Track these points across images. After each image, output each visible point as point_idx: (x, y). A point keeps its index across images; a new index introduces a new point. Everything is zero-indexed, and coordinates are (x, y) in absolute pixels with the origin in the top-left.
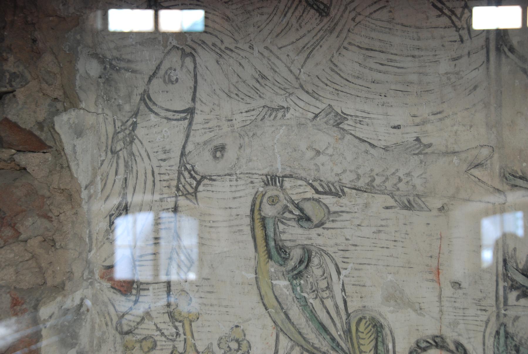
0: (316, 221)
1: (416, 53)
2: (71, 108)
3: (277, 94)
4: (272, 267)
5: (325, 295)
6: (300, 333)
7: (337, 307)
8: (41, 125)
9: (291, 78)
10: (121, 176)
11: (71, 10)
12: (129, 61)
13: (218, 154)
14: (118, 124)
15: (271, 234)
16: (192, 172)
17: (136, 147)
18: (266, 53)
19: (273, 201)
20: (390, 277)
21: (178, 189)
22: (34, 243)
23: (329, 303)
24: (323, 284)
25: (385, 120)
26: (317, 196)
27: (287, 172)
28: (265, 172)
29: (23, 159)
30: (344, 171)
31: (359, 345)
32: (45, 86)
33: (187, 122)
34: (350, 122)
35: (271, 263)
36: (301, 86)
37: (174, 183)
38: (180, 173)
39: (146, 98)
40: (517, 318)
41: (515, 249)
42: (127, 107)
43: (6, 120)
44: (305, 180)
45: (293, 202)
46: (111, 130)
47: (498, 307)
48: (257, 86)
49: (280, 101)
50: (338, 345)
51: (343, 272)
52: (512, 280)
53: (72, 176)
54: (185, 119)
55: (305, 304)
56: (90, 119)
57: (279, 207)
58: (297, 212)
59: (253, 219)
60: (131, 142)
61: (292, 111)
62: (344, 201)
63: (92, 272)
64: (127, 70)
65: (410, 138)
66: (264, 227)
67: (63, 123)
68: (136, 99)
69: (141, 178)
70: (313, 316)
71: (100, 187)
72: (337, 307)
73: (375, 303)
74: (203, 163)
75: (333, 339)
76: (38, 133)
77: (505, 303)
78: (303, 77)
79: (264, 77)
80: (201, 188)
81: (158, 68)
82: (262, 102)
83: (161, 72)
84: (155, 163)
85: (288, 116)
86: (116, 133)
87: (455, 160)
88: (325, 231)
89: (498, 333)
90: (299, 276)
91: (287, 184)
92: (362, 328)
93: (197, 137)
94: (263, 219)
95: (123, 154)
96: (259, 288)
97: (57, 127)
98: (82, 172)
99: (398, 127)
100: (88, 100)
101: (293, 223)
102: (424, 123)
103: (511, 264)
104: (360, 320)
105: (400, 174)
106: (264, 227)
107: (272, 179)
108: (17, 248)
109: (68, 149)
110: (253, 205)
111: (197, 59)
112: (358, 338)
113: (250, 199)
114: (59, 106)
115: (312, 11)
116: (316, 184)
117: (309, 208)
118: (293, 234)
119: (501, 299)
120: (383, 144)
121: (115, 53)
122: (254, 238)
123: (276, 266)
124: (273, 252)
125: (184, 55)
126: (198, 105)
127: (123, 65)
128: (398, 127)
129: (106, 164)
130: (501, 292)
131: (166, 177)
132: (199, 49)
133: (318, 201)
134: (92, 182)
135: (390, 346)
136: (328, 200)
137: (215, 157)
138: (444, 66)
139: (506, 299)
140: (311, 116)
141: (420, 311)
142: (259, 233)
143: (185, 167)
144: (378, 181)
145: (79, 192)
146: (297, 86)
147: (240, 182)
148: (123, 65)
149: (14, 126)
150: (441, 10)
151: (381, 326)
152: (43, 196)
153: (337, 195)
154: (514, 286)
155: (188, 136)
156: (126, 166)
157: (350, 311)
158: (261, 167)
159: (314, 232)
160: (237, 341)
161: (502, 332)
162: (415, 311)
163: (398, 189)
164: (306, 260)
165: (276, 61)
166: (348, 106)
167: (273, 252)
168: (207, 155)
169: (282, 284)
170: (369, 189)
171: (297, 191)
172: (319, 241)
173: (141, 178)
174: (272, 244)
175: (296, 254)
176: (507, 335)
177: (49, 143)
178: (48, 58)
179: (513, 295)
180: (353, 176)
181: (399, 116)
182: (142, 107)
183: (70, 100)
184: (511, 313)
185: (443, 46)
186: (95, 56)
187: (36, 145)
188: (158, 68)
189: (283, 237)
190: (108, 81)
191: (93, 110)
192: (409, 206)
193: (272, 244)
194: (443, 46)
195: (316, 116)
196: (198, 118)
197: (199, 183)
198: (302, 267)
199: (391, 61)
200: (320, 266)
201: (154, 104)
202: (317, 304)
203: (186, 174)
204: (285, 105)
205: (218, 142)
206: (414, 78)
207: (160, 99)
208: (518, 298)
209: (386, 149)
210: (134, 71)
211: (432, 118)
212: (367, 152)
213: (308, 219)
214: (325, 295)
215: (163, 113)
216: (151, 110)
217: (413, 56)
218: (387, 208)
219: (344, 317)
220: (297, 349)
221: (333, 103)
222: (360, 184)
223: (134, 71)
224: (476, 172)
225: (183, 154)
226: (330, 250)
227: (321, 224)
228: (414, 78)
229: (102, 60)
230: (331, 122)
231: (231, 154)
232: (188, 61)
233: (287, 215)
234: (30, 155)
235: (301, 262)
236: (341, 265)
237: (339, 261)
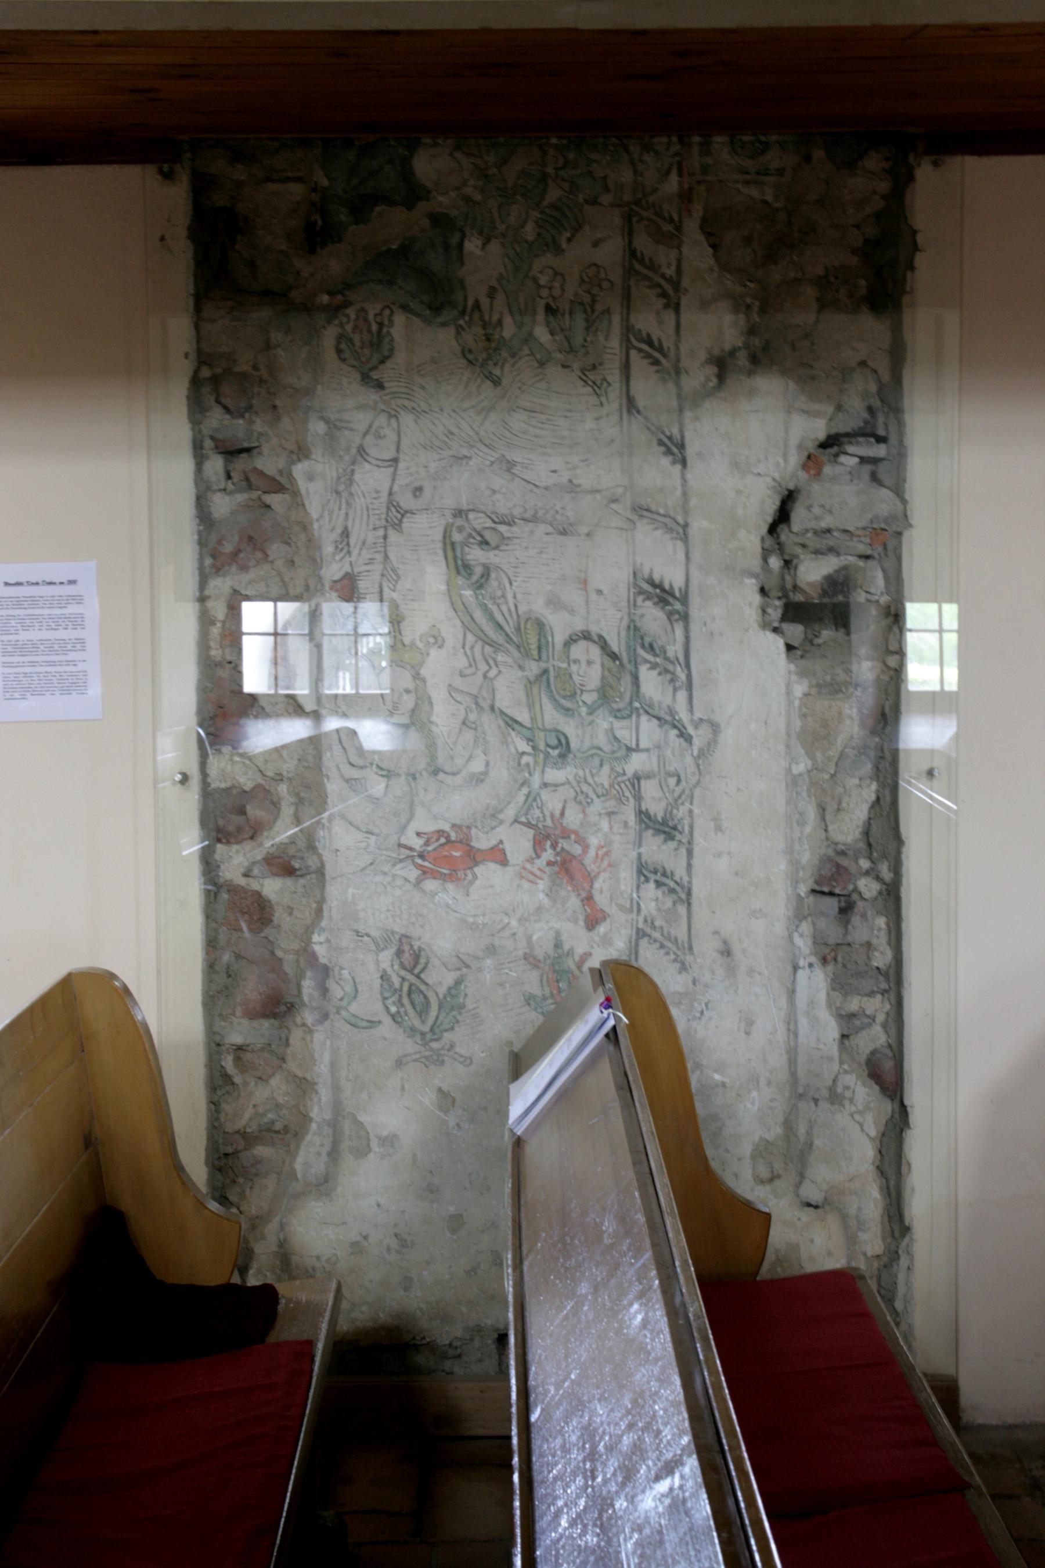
0: (493, 544)
1: (569, 414)
2: (764, 621)
3: (462, 446)
4: (460, 581)
5: (500, 601)
6: (482, 631)
7: (509, 610)
8: (281, 472)
9: (471, 433)
10: (343, 512)
11: (304, 383)
12: (348, 422)
13: (418, 494)
14: (341, 471)
15: (459, 554)
16: (397, 507)
17: (355, 488)
18: (453, 414)
19: (460, 529)
20: (550, 587)
21: (387, 521)
22: (279, 563)
23: (504, 608)
24: (499, 593)
25: (546, 468)
26: (493, 525)
27: (471, 507)
28: (453, 507)
29: (269, 499)
30: (515, 506)
31: (527, 638)
32: (283, 442)
33: (392, 469)
34: (519, 468)
35: (460, 578)
36: (481, 441)
37: (383, 516)
38: (388, 509)
39: (362, 451)
40: (642, 616)
41: (642, 564)
42: (347, 458)
43: (255, 469)
44: (485, 513)
45: (475, 530)
46: (335, 475)
47: (629, 607)
48: (447, 440)
49: (465, 452)
50: (511, 639)
51: (515, 584)
52: (640, 587)
53: (306, 511)
54: (391, 466)
55: (485, 609)
56: (319, 468)
57: (465, 534)
58: (479, 538)
59: (445, 544)
60: (351, 485)
61: (474, 460)
62: (515, 529)
63: (323, 585)
64: (346, 428)
65: (564, 480)
66: (454, 550)
67: (299, 470)
68: (354, 451)
69: (359, 512)
70: (491, 618)
71: (327, 519)
72: (509, 610)
73: (539, 607)
74: (406, 501)
75: (507, 635)
76: (278, 478)
77: (635, 605)
78: (482, 433)
79: (452, 433)
80: (405, 520)
81: (370, 426)
82: (451, 453)
83: (373, 430)
84: (369, 500)
85: (471, 463)
86: (339, 478)
87: (598, 496)
88: (501, 553)
89: (629, 627)
90: (481, 587)
91: (471, 516)
92: (529, 626)
93: (401, 481)
94: (453, 544)
95: (345, 494)
96: (450, 597)
97: (294, 474)
98: (314, 508)
99: (555, 471)
100: (317, 453)
101: (476, 547)
102: (575, 468)
103: (639, 575)
104: (527, 620)
105: (557, 508)
106: (454, 550)
107: (459, 513)
108: (266, 567)
109: (303, 491)
110: (445, 532)
111: (401, 420)
112: (526, 633)
113: (441, 529)
114: (295, 457)
115: (489, 382)
116: (494, 517)
117: (488, 535)
118: (476, 555)
119: (632, 602)
120: (543, 484)
121: (337, 416)
122: (446, 558)
123: (464, 580)
124: (461, 568)
125: (390, 416)
126: (401, 456)
127: (343, 424)
128: (555, 471)
129: (332, 502)
130: (632, 597)
131: (378, 512)
132: (402, 412)
133: (495, 529)
134: (321, 516)
135: (550, 639)
136: (502, 528)
137: (415, 496)
138: (589, 424)
139: (635, 601)
140: (488, 463)
141: (572, 612)
142: (450, 554)
143: (392, 503)
144: (541, 513)
145: (311, 524)
146: (476, 439)
147: (435, 515)
148: (343, 424)
149: (261, 473)
150: (585, 381)
151: (544, 624)
152: (284, 528)
153: (509, 524)
154: (641, 592)
155: (393, 480)
156: (347, 503)
157: (520, 613)
158: (450, 502)
159: (492, 554)
160: (434, 637)
161: (632, 627)
162: (569, 612)
163: (556, 520)
164: (486, 575)
165: (462, 422)
166: (517, 456)
167: (461, 568)
168: (409, 495)
169: (468, 593)
170: (534, 519)
171: (479, 521)
172: (496, 560)
173: (359, 512)
174: (460, 563)
175: (478, 570)
176: (636, 629)
177: (288, 486)
178: (286, 420)
179: (640, 599)
180: (521, 510)
181: (556, 463)
182: (359, 458)
183: (301, 452)
184: (639, 612)
185: (426, 467)
186: (322, 418)
187: (278, 487)
188: (370, 426)
189: (468, 557)
190: (332, 438)
191: (320, 460)
192: (564, 533)
193: (460, 563)
194: (426, 467)
195: (492, 463)
196: (402, 465)
197: (403, 516)
198: (483, 580)
199: (549, 420)
200: (497, 579)
201: (368, 455)
202: (494, 608)
203: (393, 509)
204: (468, 454)
205: (417, 484)
206: (566, 433)
207: (372, 451)
208: (644, 601)
209: (546, 488)
210: (351, 430)
211: (581, 464)
212: (531, 491)
213: (487, 543)
214: (500, 601)
215: (374, 462)
216: (365, 460)
217: (566, 417)
218: (547, 534)
219: (515, 617)
220: (480, 643)
221: (505, 453)
222: (527, 515)
223: (351, 430)
224: (614, 506)
225: (390, 494)
226: (504, 567)
227: (497, 548)
228: (566, 433)
229: (327, 421)
230: (504, 468)
231: (427, 493)
232: (393, 421)
233: (472, 540)
234: (273, 495)
235: (482, 576)
236: (513, 578)
237: (510, 575)
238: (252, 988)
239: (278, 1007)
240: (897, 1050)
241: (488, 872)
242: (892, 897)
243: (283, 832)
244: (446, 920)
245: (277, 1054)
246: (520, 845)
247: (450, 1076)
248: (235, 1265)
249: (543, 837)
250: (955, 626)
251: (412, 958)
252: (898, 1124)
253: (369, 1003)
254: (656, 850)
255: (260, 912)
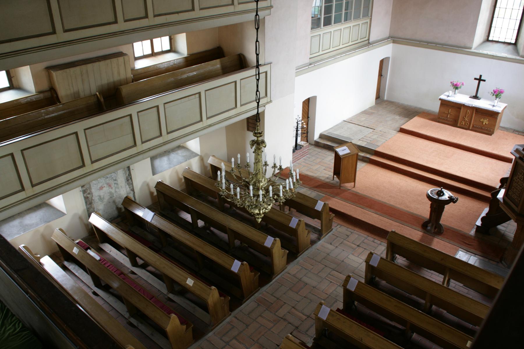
146: (67, 85)
238: (88, 203)
239: (91, 203)
240: (133, 188)
241: (104, 188)
242: (131, 178)
243: (88, 191)
244: (101, 193)
245: (91, 207)
246: (106, 185)
247: (104, 203)
248: (358, 256)
249: (107, 184)
250: (147, 43)
251: (100, 196)
252: (134, 193)
253: (98, 201)
254: (115, 182)
255: (88, 197)
